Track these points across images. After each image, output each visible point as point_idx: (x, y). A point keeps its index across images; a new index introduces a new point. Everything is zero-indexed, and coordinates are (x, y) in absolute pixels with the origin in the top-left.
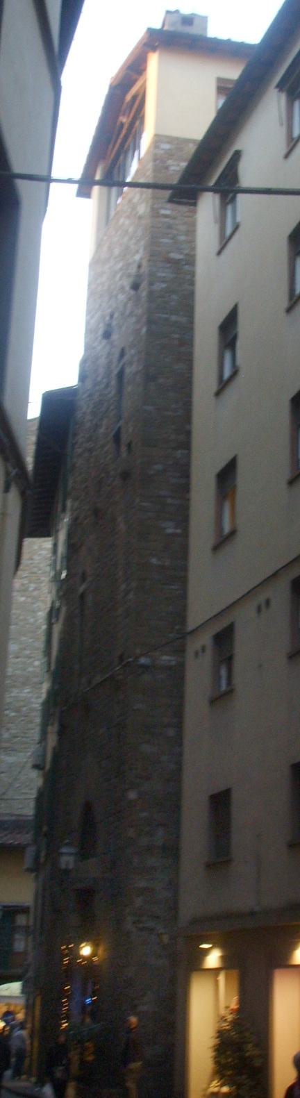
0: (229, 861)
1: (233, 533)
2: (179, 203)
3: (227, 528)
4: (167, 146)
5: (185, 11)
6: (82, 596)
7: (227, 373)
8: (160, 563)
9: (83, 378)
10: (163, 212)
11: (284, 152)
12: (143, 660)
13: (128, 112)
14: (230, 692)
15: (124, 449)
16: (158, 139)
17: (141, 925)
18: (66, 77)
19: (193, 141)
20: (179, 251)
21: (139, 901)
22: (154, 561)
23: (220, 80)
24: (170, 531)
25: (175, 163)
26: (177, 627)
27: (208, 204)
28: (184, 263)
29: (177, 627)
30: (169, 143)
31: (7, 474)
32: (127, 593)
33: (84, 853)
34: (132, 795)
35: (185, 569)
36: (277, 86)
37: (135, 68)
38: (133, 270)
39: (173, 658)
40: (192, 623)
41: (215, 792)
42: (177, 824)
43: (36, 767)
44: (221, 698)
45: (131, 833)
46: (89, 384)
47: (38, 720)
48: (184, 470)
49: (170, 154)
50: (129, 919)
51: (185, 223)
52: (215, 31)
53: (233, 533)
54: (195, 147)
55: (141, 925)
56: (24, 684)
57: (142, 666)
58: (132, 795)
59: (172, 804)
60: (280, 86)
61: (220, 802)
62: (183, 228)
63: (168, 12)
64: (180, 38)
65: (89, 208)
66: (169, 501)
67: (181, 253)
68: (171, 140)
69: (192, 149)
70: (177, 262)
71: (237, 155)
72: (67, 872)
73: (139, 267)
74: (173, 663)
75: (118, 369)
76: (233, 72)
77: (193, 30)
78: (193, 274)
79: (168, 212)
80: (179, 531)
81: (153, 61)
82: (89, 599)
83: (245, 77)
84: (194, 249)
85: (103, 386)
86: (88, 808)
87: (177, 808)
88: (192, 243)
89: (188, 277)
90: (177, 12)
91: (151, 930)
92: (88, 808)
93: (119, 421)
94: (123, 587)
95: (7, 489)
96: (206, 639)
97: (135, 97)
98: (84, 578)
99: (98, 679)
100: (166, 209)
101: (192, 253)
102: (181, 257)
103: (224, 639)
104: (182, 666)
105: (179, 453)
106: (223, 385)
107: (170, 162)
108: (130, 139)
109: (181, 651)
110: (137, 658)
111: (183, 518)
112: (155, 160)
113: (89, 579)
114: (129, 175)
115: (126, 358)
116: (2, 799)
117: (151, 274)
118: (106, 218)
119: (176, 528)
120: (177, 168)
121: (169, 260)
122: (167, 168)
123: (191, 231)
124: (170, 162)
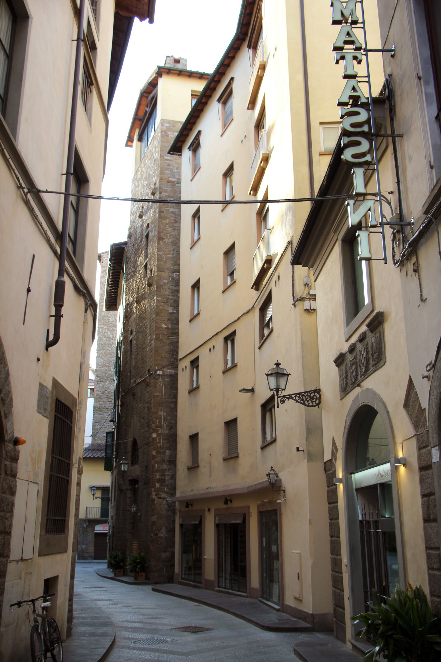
3: (196, 312)
4: (167, 125)
5: (177, 57)
6: (131, 341)
8: (166, 327)
9: (130, 236)
10: (166, 158)
11: (221, 133)
12: (159, 372)
14: (198, 387)
15: (149, 272)
16: (163, 122)
17: (159, 496)
18: (111, 115)
19: (180, 122)
20: (174, 177)
21: (158, 485)
24: (170, 311)
25: (172, 133)
26: (175, 356)
27: (186, 154)
28: (176, 183)
30: (168, 123)
31: (86, 304)
32: (151, 340)
33: (134, 461)
34: (154, 435)
35: (178, 329)
37: (153, 85)
38: (152, 187)
39: (173, 371)
40: (180, 356)
42: (175, 449)
43: (111, 421)
44: (193, 390)
45: (154, 453)
46: (133, 239)
47: (113, 397)
48: (177, 283)
49: (169, 129)
50: (154, 493)
51: (176, 163)
52: (190, 68)
53: (198, 314)
54: (182, 125)
55: (159, 496)
56: (106, 380)
57: (159, 375)
58: (154, 435)
59: (172, 438)
62: (176, 166)
63: (167, 57)
64: (174, 69)
67: (174, 178)
68: (169, 122)
69: (180, 126)
70: (173, 182)
72: (125, 472)
73: (155, 184)
74: (173, 373)
77: (179, 66)
78: (180, 188)
80: (175, 311)
82: (134, 342)
84: (180, 176)
85: (139, 241)
86: (135, 442)
88: (179, 173)
89: (179, 189)
90: (172, 56)
92: (135, 442)
95: (86, 311)
96: (186, 363)
97: (152, 98)
98: (132, 333)
99: (139, 381)
100: (167, 156)
103: (195, 363)
104: (177, 374)
106: (194, 243)
107: (169, 133)
109: (176, 367)
110: (156, 372)
112: (162, 132)
113: (134, 333)
115: (149, 228)
117: (160, 188)
118: (140, 158)
119: (173, 310)
121: (169, 182)
122: (168, 136)
124: (169, 133)
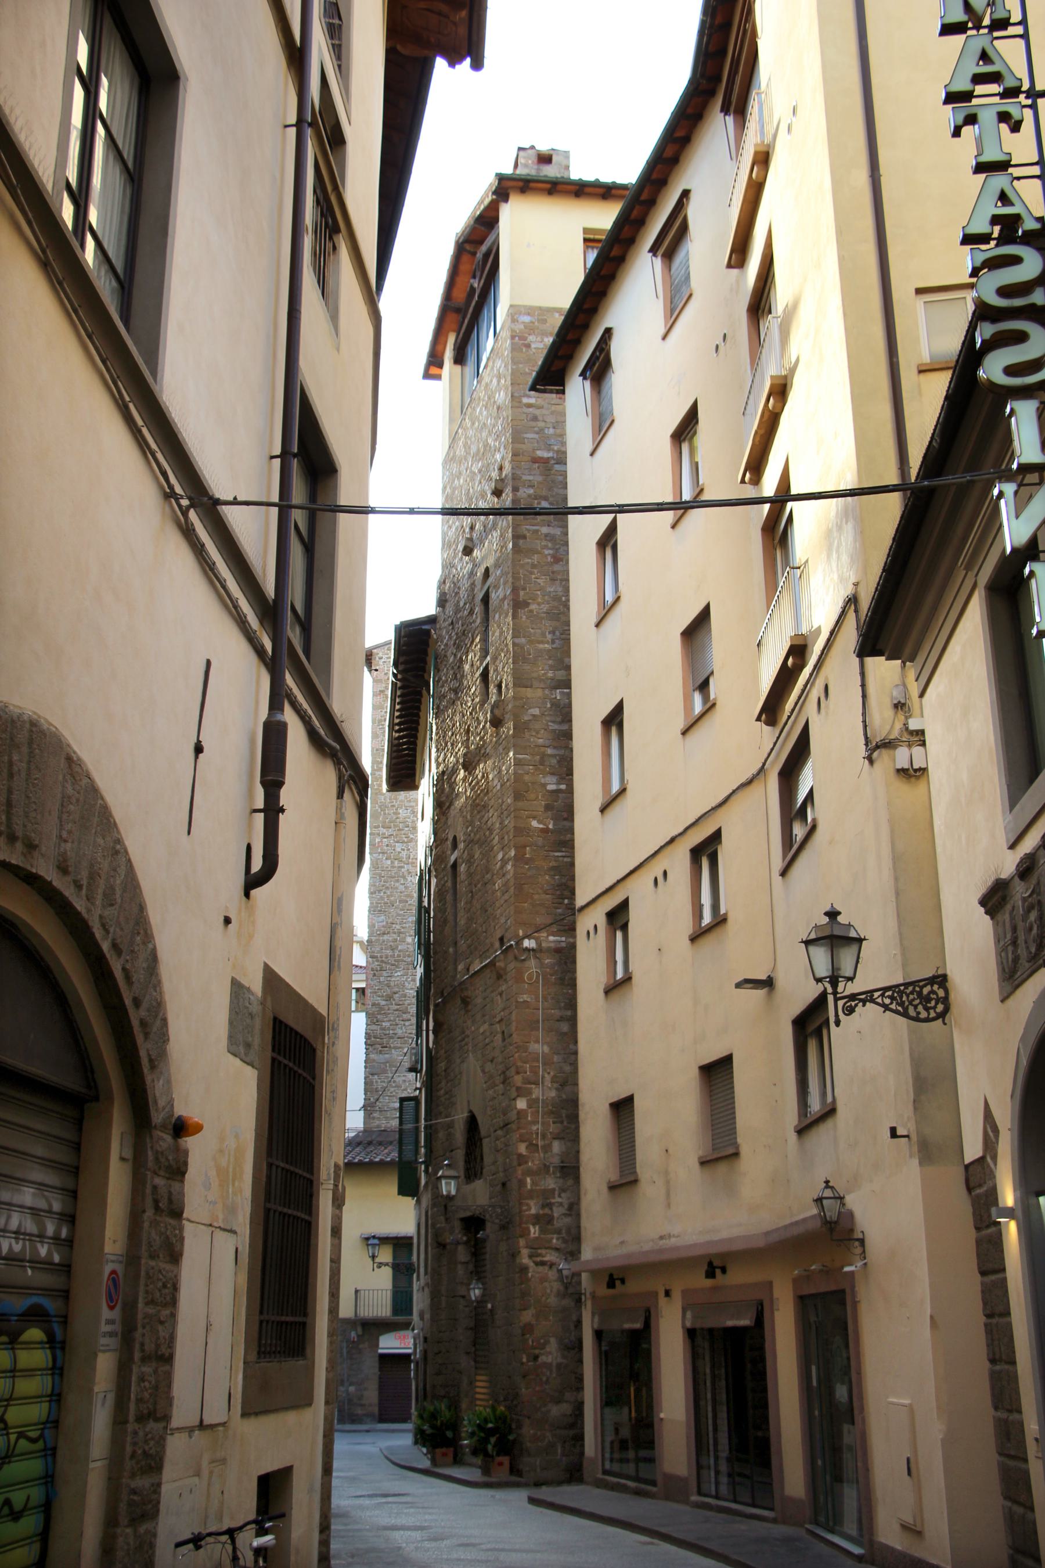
0: (635, 1181)
1: (623, 791)
2: (544, 391)
4: (527, 319)
5: (543, 147)
6: (455, 866)
7: (609, 598)
8: (541, 826)
9: (442, 602)
10: (525, 400)
11: (662, 331)
12: (526, 943)
13: (478, 274)
14: (628, 979)
15: (493, 689)
16: (515, 312)
19: (558, 310)
21: (534, 1231)
22: (535, 824)
23: (586, 231)
29: (566, 901)
30: (529, 314)
31: (340, 777)
32: (504, 862)
33: (472, 1170)
34: (521, 1104)
35: (571, 830)
36: (650, 251)
40: (580, 901)
41: (615, 1099)
43: (412, 1070)
44: (617, 986)
46: (450, 609)
48: (564, 713)
49: (530, 329)
50: (525, 1252)
51: (552, 413)
53: (623, 791)
55: (538, 1259)
57: (527, 950)
58: (521, 1104)
59: (567, 1112)
60: (654, 250)
61: (622, 1109)
62: (551, 419)
63: (520, 149)
64: (538, 179)
65: (437, 394)
66: (549, 751)
67: (549, 450)
68: (530, 311)
69: (558, 320)
70: (546, 461)
71: (608, 332)
72: (450, 1198)
73: (501, 469)
75: (483, 592)
76: (604, 217)
77: (550, 171)
79: (532, 401)
80: (563, 787)
81: (510, 214)
82: (462, 868)
83: (621, 223)
84: (564, 444)
86: (472, 1123)
87: (573, 1118)
89: (560, 478)
90: (533, 147)
91: (552, 1265)
92: (472, 1123)
93: (486, 657)
94: (500, 856)
95: (340, 795)
97: (487, 255)
99: (477, 966)
100: (529, 397)
101: (563, 449)
102: (550, 455)
104: (573, 947)
105: (558, 694)
106: (606, 611)
107: (531, 338)
108: (340, 933)
109: (571, 929)
110: (519, 942)
111: (565, 769)
112: (513, 338)
113: (461, 846)
114: (485, 349)
115: (491, 580)
116: (324, 1558)
117: (515, 477)
118: (461, 407)
119: (558, 783)
120: (541, 346)
121: (535, 460)
122: (528, 346)
123: (560, 423)
